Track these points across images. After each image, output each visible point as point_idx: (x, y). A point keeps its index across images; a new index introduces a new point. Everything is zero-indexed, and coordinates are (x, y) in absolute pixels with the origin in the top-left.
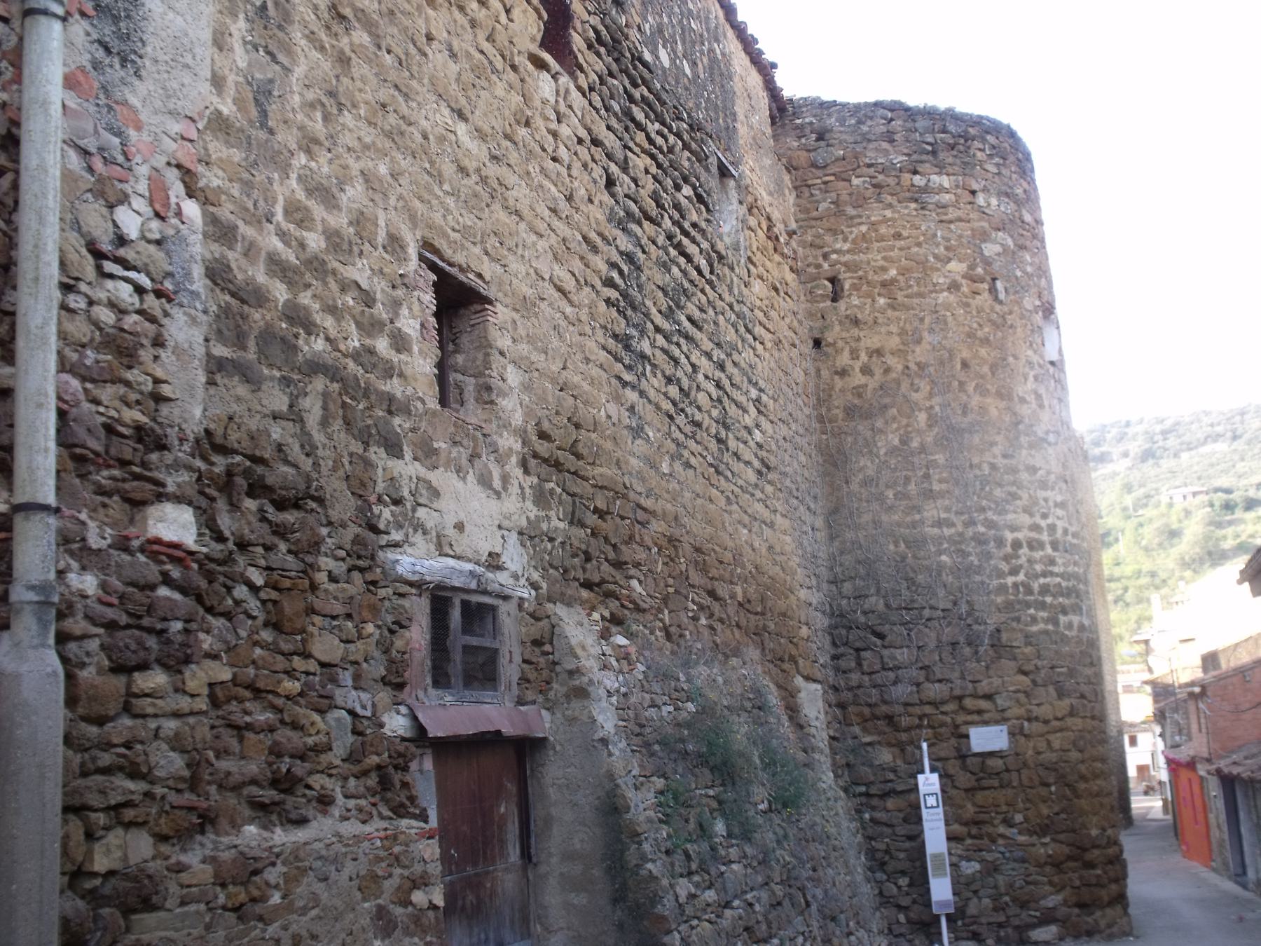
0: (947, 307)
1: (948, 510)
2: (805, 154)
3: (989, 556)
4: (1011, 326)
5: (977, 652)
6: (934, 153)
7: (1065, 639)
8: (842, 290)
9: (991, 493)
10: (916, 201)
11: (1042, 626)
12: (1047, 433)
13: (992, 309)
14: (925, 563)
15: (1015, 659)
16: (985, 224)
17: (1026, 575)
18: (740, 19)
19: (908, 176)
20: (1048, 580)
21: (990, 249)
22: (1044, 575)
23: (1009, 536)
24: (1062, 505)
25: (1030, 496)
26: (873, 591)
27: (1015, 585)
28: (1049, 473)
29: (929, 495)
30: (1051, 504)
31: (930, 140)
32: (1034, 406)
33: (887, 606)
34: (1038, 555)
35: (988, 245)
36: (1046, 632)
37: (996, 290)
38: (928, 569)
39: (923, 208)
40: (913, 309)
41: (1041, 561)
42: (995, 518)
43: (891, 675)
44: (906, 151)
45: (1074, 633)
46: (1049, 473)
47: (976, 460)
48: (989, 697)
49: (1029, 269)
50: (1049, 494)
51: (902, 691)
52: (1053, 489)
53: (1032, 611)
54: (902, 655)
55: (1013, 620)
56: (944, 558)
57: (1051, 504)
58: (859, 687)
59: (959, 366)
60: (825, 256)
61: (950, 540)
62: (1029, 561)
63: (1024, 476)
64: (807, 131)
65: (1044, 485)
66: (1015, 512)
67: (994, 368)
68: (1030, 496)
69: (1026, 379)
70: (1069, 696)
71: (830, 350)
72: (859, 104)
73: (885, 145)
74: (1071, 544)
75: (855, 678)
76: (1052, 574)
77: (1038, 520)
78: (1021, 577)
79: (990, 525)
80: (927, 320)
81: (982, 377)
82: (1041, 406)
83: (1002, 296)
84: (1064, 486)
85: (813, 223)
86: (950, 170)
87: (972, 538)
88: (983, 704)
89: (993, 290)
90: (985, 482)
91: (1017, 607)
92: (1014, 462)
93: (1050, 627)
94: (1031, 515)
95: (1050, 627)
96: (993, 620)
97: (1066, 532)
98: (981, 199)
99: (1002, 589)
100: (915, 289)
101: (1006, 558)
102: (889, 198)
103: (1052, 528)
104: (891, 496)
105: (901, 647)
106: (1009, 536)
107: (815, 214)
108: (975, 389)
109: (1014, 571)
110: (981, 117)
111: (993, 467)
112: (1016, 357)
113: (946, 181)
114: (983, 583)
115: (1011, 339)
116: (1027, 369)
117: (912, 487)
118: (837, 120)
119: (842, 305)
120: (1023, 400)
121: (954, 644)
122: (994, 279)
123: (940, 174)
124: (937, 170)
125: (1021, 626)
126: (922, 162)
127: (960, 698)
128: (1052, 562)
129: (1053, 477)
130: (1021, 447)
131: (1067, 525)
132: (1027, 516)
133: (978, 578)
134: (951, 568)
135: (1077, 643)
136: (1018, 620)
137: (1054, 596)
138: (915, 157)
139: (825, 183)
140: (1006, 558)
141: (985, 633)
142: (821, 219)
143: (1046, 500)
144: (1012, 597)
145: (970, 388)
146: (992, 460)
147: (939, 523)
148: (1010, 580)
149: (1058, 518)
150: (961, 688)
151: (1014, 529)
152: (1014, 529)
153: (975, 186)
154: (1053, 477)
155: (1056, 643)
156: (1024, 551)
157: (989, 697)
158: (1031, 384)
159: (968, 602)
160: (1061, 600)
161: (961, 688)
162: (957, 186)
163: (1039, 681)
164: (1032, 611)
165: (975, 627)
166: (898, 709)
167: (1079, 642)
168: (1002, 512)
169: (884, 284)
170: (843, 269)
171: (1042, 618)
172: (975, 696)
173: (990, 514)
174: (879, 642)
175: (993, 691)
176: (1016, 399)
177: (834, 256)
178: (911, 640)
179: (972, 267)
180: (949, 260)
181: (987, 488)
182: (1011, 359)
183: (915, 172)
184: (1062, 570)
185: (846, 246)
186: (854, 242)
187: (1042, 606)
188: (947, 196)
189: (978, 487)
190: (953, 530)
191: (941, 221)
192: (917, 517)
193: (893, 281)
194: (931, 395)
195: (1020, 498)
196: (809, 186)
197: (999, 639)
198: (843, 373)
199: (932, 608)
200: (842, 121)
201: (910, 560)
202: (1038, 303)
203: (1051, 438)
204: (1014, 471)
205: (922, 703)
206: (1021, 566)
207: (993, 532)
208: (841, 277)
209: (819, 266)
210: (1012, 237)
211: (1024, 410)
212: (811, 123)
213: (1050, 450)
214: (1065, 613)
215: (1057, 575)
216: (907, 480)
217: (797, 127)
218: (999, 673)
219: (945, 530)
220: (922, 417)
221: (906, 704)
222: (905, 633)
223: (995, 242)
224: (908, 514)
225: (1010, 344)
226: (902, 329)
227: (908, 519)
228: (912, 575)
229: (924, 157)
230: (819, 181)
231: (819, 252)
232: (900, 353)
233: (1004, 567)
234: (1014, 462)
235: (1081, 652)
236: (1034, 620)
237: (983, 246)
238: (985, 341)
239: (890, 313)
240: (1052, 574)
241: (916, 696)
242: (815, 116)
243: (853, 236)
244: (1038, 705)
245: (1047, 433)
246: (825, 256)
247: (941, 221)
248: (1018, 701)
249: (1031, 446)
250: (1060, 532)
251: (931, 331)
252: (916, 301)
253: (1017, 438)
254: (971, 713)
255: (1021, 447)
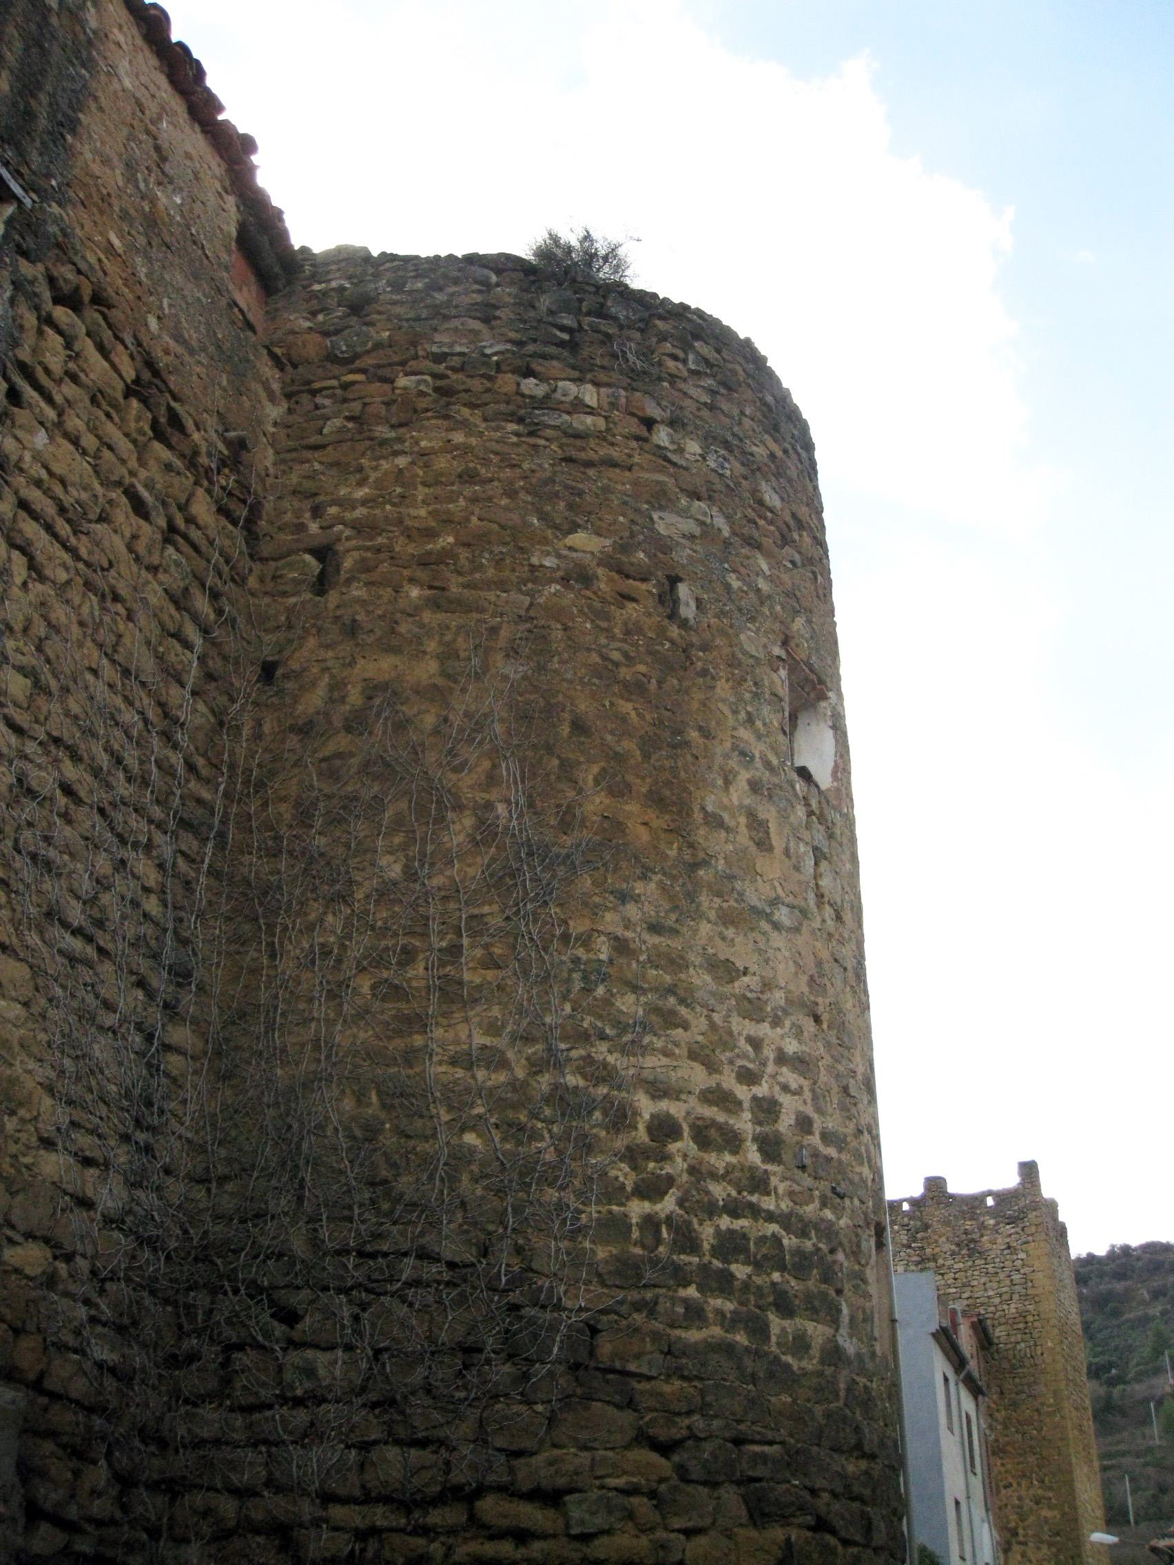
0: (557, 613)
1: (493, 1029)
2: (317, 338)
3: (587, 1146)
4: (704, 673)
5: (526, 1377)
6: (573, 346)
7: (779, 1375)
8: (338, 571)
9: (608, 1002)
10: (521, 420)
11: (716, 1331)
12: (775, 902)
13: (662, 632)
14: (423, 1147)
15: (630, 1404)
16: (670, 482)
17: (681, 1203)
18: (375, 253)
19: (510, 378)
20: (742, 1223)
21: (667, 524)
22: (734, 1210)
23: (646, 1107)
24: (801, 1064)
25: (713, 1026)
26: (284, 1202)
27: (650, 1222)
28: (767, 986)
29: (452, 994)
30: (769, 1053)
31: (568, 321)
32: (743, 837)
33: (315, 1243)
34: (720, 1160)
35: (671, 518)
36: (728, 1349)
37: (676, 602)
38: (427, 1161)
39: (531, 434)
40: (481, 610)
41: (726, 1176)
42: (611, 1059)
43: (301, 1417)
44: (513, 335)
45: (810, 1364)
46: (767, 986)
47: (578, 927)
48: (551, 1498)
49: (762, 584)
50: (764, 1030)
51: (316, 1461)
52: (776, 1022)
53: (691, 1292)
54: (331, 1367)
55: (638, 1306)
56: (470, 1138)
57: (769, 1053)
58: (217, 1442)
59: (565, 730)
60: (317, 512)
61: (497, 1102)
62: (692, 1170)
63: (701, 979)
64: (332, 302)
65: (752, 1008)
66: (666, 1054)
67: (649, 745)
68: (713, 1026)
69: (727, 783)
70: (785, 1520)
71: (290, 685)
72: (437, 258)
73: (476, 325)
74: (815, 1154)
75: (211, 1419)
76: (755, 1212)
77: (728, 1081)
78: (668, 1205)
79: (605, 1074)
80: (504, 633)
81: (619, 758)
82: (764, 845)
83: (688, 611)
84: (809, 1025)
85: (308, 454)
86: (603, 377)
87: (548, 1100)
88: (533, 1515)
89: (668, 599)
90: (594, 974)
91: (649, 1275)
92: (676, 944)
93: (741, 1338)
94: (712, 1067)
95: (741, 1338)
96: (581, 1299)
97: (804, 1124)
98: (662, 436)
99: (616, 1227)
100: (491, 572)
101: (633, 1156)
102: (466, 411)
103: (767, 1109)
104: (366, 989)
105: (331, 1348)
106: (646, 1107)
107: (314, 439)
108: (597, 782)
109: (652, 1189)
110: (684, 307)
111: (621, 947)
112: (706, 733)
113: (590, 395)
114: (561, 1206)
115: (698, 695)
116: (733, 763)
117: (417, 971)
118: (389, 283)
119: (333, 598)
120: (715, 822)
121: (469, 1350)
122: (674, 580)
123: (579, 381)
124: (576, 374)
125: (658, 1326)
126: (544, 357)
127: (467, 1496)
128: (760, 1184)
129: (778, 997)
130: (698, 915)
131: (809, 1110)
132: (698, 1068)
133: (552, 1195)
134: (483, 1165)
135: (819, 1390)
136: (650, 1308)
137: (758, 1265)
138: (531, 348)
139: (345, 386)
140: (633, 1156)
141: (553, 1328)
142: (322, 447)
143: (756, 1043)
144: (638, 1251)
145: (588, 775)
146: (620, 932)
147: (464, 1060)
148: (637, 1209)
149: (785, 1088)
150: (473, 1467)
151: (659, 1090)
152: (659, 1090)
153: (652, 410)
154: (778, 997)
155: (754, 1378)
156: (685, 1145)
157: (551, 1498)
158: (739, 794)
159: (519, 1250)
160: (776, 1276)
161: (473, 1467)
162: (613, 405)
163: (696, 1472)
164: (691, 1292)
165: (529, 1312)
166: (307, 1509)
167: (826, 1389)
168: (634, 1049)
169: (424, 562)
170: (348, 532)
171: (720, 1312)
172: (507, 1490)
173: (601, 1051)
174: (279, 1329)
175: (561, 1482)
176: (698, 816)
177: (333, 510)
178: (359, 1333)
179: (625, 548)
180: (574, 528)
181: (600, 991)
182: (694, 735)
183: (528, 373)
184: (785, 1205)
185: (360, 493)
186: (379, 485)
187: (724, 1284)
188: (589, 420)
189: (578, 985)
190: (502, 1077)
191: (569, 460)
192: (418, 1040)
193: (445, 556)
194: (492, 780)
195: (686, 1026)
196: (314, 393)
197: (592, 1353)
198: (305, 730)
199: (425, 1255)
200: (397, 286)
201: (388, 1140)
202: (777, 651)
203: (783, 915)
204: (677, 963)
205: (367, 1499)
206: (670, 1180)
207: (603, 1090)
208: (340, 548)
209: (301, 527)
210: (728, 518)
211: (717, 844)
212: (342, 289)
213: (778, 940)
214: (785, 1307)
215: (770, 1217)
216: (408, 955)
217: (314, 295)
218: (583, 1436)
219: (481, 1074)
220: (460, 829)
221: (328, 1498)
222: (346, 1312)
223: (684, 513)
224: (399, 1033)
225: (695, 705)
226: (448, 644)
227: (398, 1043)
228: (384, 1173)
229: (551, 350)
230: (334, 383)
231: (307, 504)
232: (436, 694)
233: (624, 1174)
234: (676, 944)
235: (828, 1415)
236: (695, 1314)
237: (655, 516)
238: (636, 689)
239: (427, 616)
240: (755, 1212)
241: (353, 1477)
242: (349, 278)
243: (378, 474)
244: (688, 1533)
245: (775, 902)
246: (317, 512)
247: (569, 460)
248: (630, 1515)
249: (727, 919)
250: (785, 1124)
251: (512, 652)
252: (491, 596)
253: (691, 896)
254: (497, 1535)
255: (698, 915)
